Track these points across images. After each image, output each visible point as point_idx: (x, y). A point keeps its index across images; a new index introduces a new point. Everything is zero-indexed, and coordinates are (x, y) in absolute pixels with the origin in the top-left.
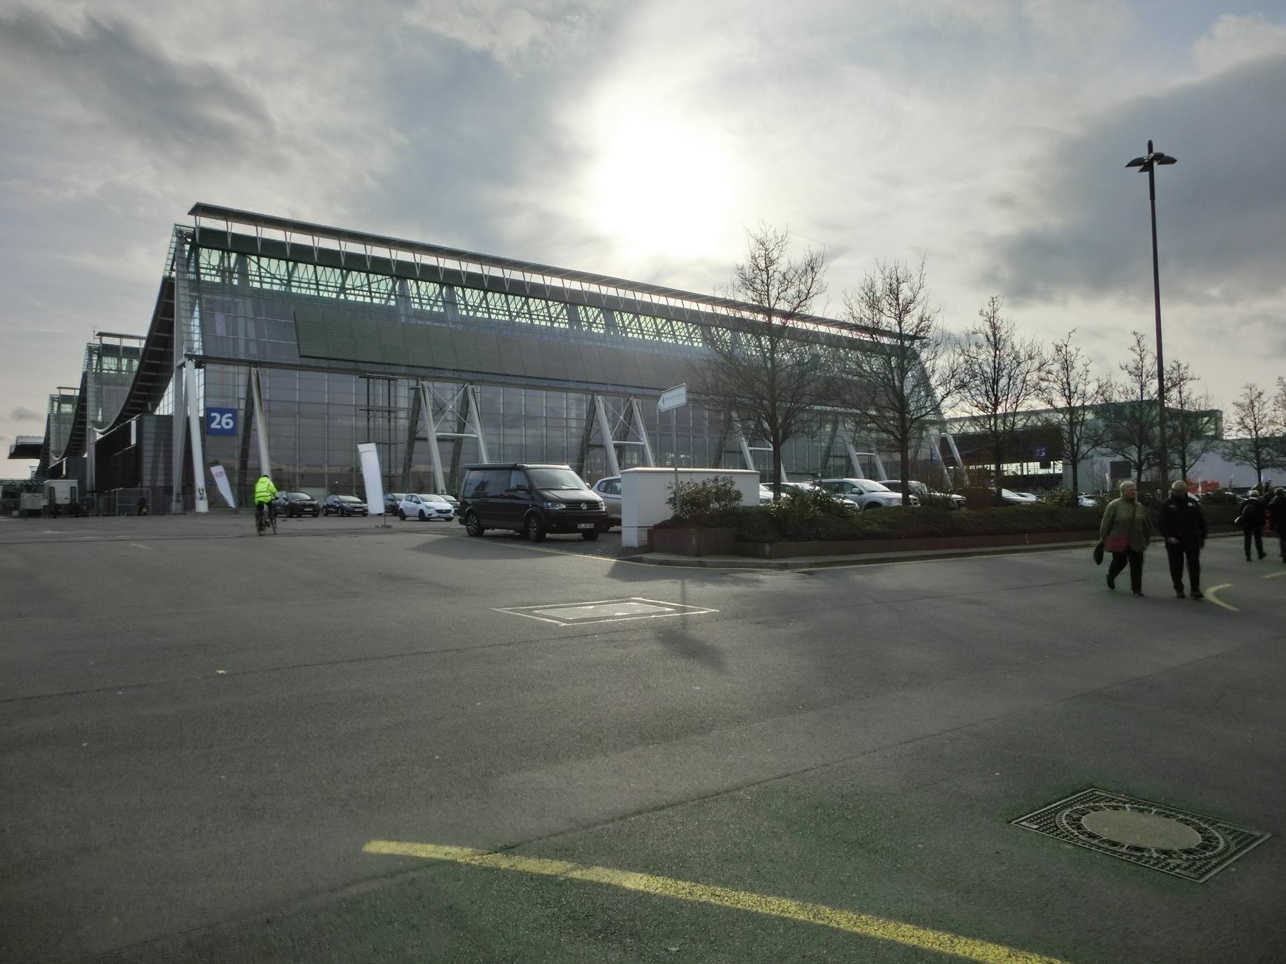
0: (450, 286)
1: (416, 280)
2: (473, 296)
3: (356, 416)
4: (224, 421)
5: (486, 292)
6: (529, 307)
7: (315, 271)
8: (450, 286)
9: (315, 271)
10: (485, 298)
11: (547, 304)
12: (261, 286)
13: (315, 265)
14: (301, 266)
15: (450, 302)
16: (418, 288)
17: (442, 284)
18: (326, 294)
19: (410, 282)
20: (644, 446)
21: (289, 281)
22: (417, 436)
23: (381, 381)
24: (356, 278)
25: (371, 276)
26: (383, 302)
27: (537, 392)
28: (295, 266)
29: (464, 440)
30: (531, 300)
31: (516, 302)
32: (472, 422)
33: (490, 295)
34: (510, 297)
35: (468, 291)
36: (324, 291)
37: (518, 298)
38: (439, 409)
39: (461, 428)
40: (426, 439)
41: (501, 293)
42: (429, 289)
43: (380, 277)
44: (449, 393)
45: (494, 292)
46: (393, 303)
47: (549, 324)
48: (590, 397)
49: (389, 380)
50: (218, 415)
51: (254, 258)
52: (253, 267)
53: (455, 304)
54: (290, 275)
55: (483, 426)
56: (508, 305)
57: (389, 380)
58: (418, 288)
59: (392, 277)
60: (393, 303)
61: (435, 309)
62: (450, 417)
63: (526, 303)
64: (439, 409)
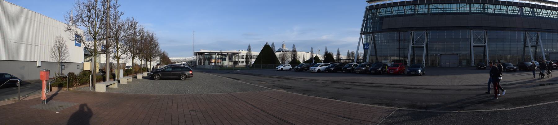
0: (533, 8)
1: (525, 7)
2: (539, 10)
3: (547, 42)
4: (367, 46)
5: (542, 9)
6: (552, 13)
7: (513, 7)
8: (533, 8)
9: (513, 7)
10: (542, 11)
11: (470, 6)
12: (533, 12)
13: (513, 6)
14: (497, 6)
15: (533, 12)
16: (525, 9)
17: (531, 8)
18: (509, 13)
19: (523, 8)
20: (541, 46)
21: (507, 10)
22: (526, 46)
23: (472, 34)
24: (510, 8)
25: (514, 7)
26: (517, 14)
27: (555, 34)
28: (508, 7)
29: (538, 46)
30: (553, 11)
31: (549, 11)
32: (539, 42)
33: (543, 10)
34: (548, 10)
35: (537, 9)
36: (491, 11)
37: (550, 11)
38: (531, 39)
39: (537, 44)
40: (528, 47)
41: (545, 9)
42: (528, 9)
43: (516, 7)
44: (534, 35)
45: (544, 9)
46: (519, 14)
47: (553, 17)
48: (525, 33)
49: (405, 32)
50: (366, 45)
51: (486, 5)
52: (486, 7)
53: (534, 13)
54: (507, 8)
55: (542, 42)
56: (547, 12)
57: (405, 32)
58: (525, 9)
59: (530, 7)
60: (519, 14)
61: (530, 15)
62: (534, 41)
63: (552, 11)
64: (531, 39)
